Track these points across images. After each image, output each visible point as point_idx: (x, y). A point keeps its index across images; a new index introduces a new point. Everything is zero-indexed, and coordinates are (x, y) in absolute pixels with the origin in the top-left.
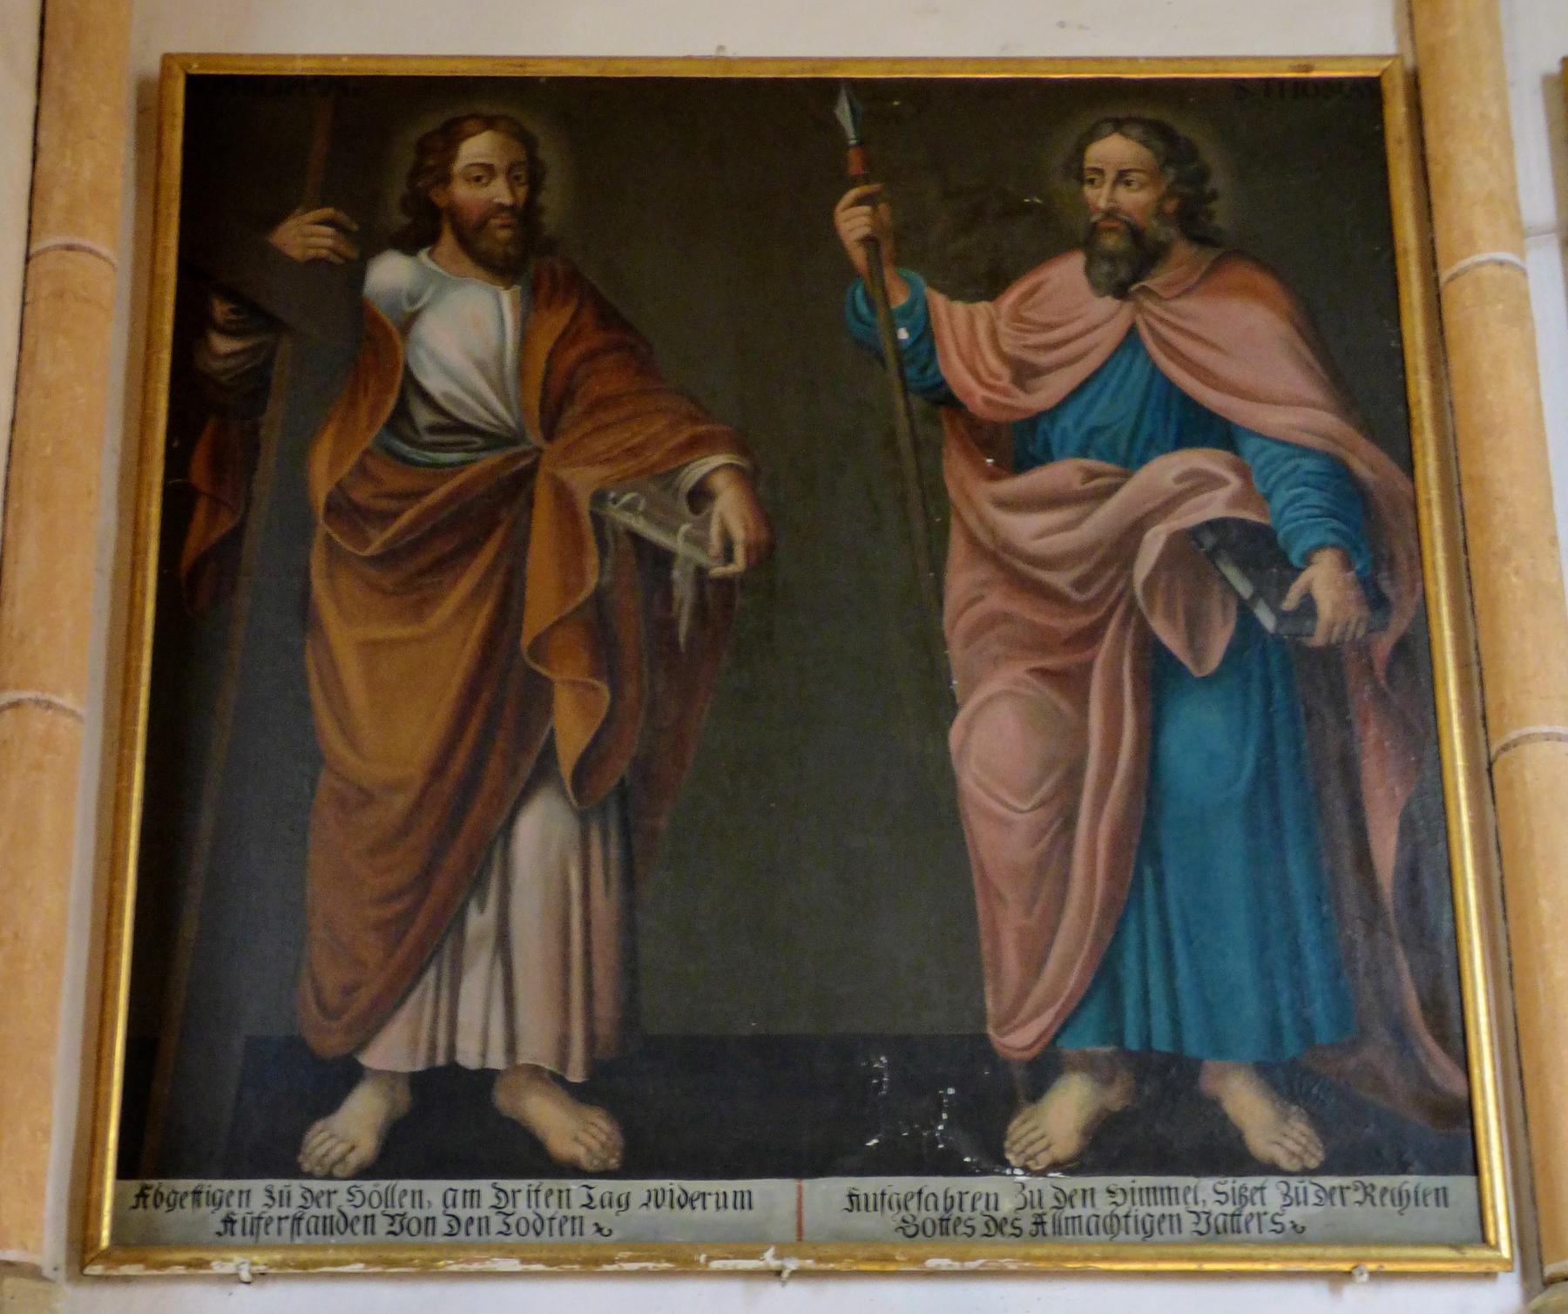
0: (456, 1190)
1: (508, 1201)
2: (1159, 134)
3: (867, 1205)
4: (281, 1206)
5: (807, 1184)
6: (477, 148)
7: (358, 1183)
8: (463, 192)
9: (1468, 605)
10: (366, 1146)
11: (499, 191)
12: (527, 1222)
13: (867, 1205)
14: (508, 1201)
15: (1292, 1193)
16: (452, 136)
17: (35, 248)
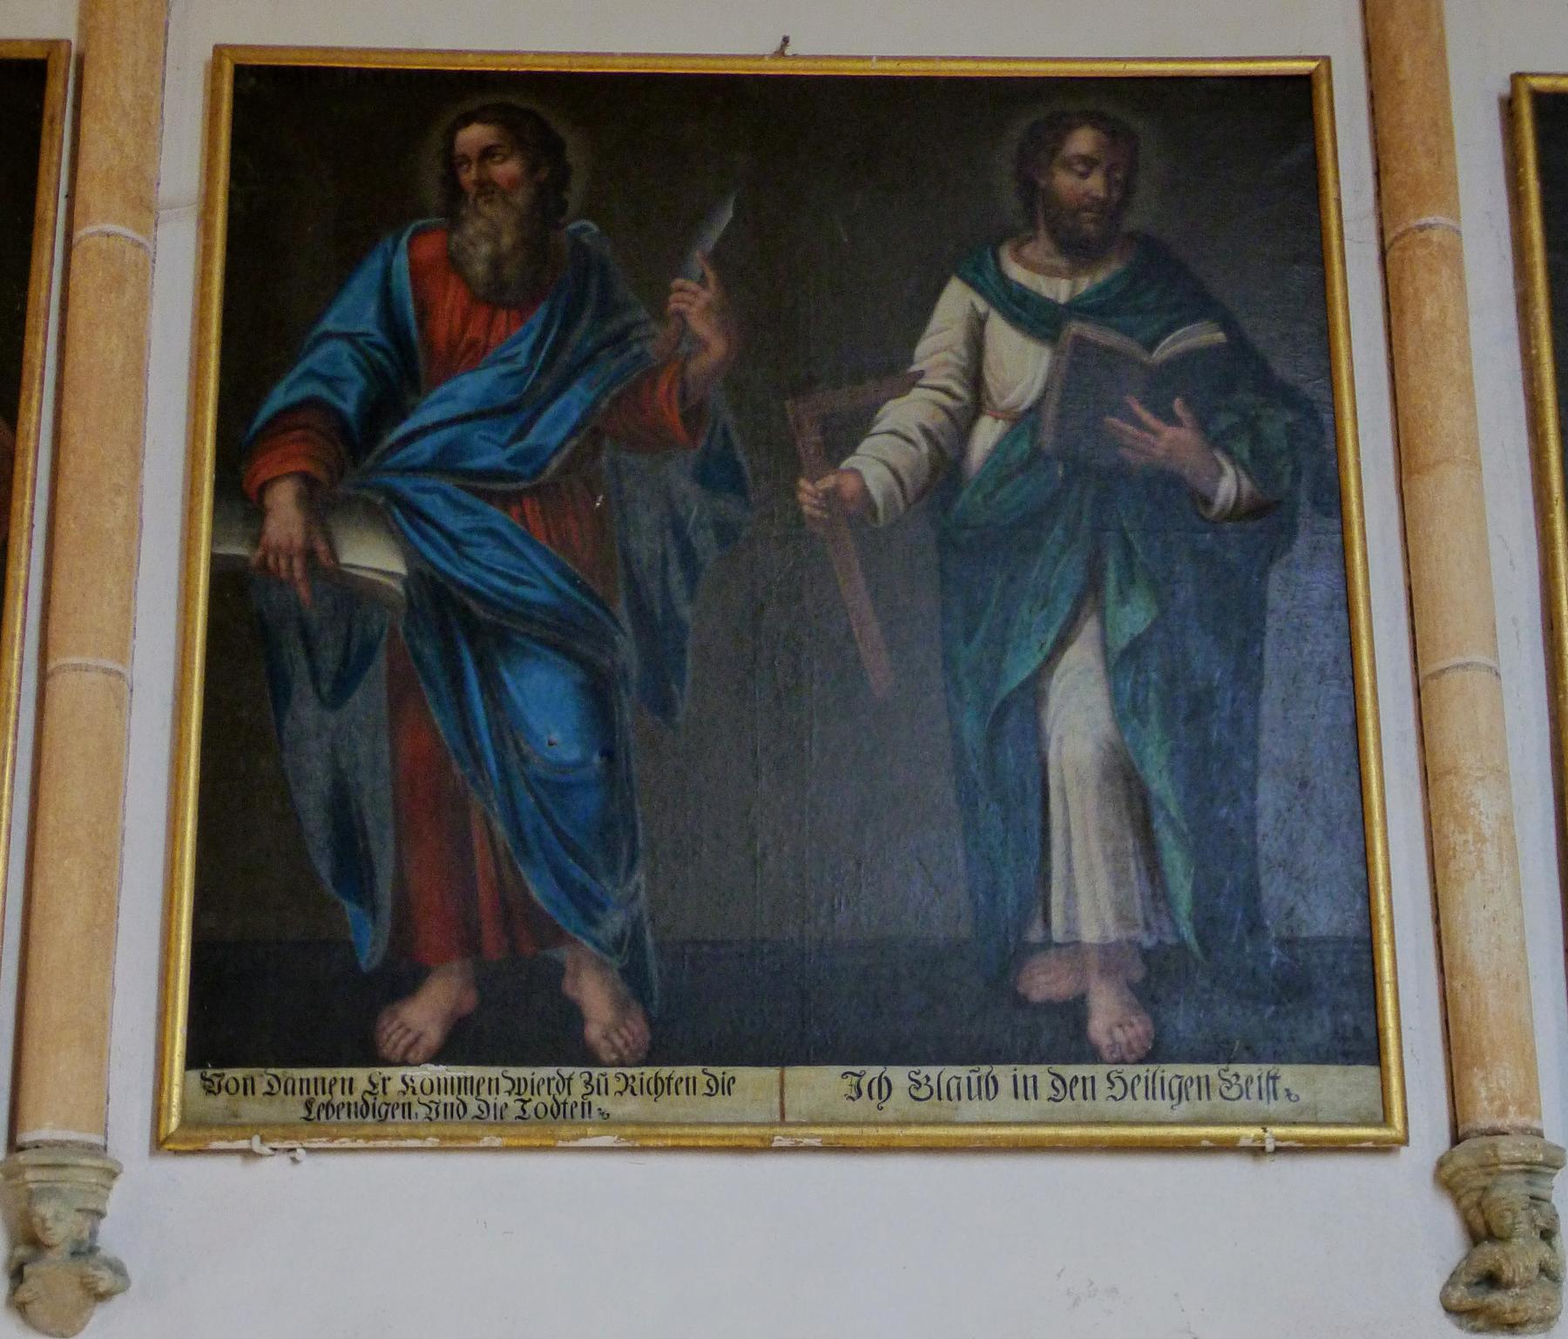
0: (960, 1078)
1: (1066, 1092)
2: (1114, 132)
3: (316, 1082)
4: (472, 1078)
5: (796, 1074)
6: (1083, 141)
7: (1119, 1067)
8: (1065, 182)
9: (22, 587)
10: (433, 1035)
11: (1095, 184)
12: (227, 1090)
13: (316, 1082)
14: (1066, 1092)
15: (594, 1082)
16: (1061, 127)
17: (1389, 237)
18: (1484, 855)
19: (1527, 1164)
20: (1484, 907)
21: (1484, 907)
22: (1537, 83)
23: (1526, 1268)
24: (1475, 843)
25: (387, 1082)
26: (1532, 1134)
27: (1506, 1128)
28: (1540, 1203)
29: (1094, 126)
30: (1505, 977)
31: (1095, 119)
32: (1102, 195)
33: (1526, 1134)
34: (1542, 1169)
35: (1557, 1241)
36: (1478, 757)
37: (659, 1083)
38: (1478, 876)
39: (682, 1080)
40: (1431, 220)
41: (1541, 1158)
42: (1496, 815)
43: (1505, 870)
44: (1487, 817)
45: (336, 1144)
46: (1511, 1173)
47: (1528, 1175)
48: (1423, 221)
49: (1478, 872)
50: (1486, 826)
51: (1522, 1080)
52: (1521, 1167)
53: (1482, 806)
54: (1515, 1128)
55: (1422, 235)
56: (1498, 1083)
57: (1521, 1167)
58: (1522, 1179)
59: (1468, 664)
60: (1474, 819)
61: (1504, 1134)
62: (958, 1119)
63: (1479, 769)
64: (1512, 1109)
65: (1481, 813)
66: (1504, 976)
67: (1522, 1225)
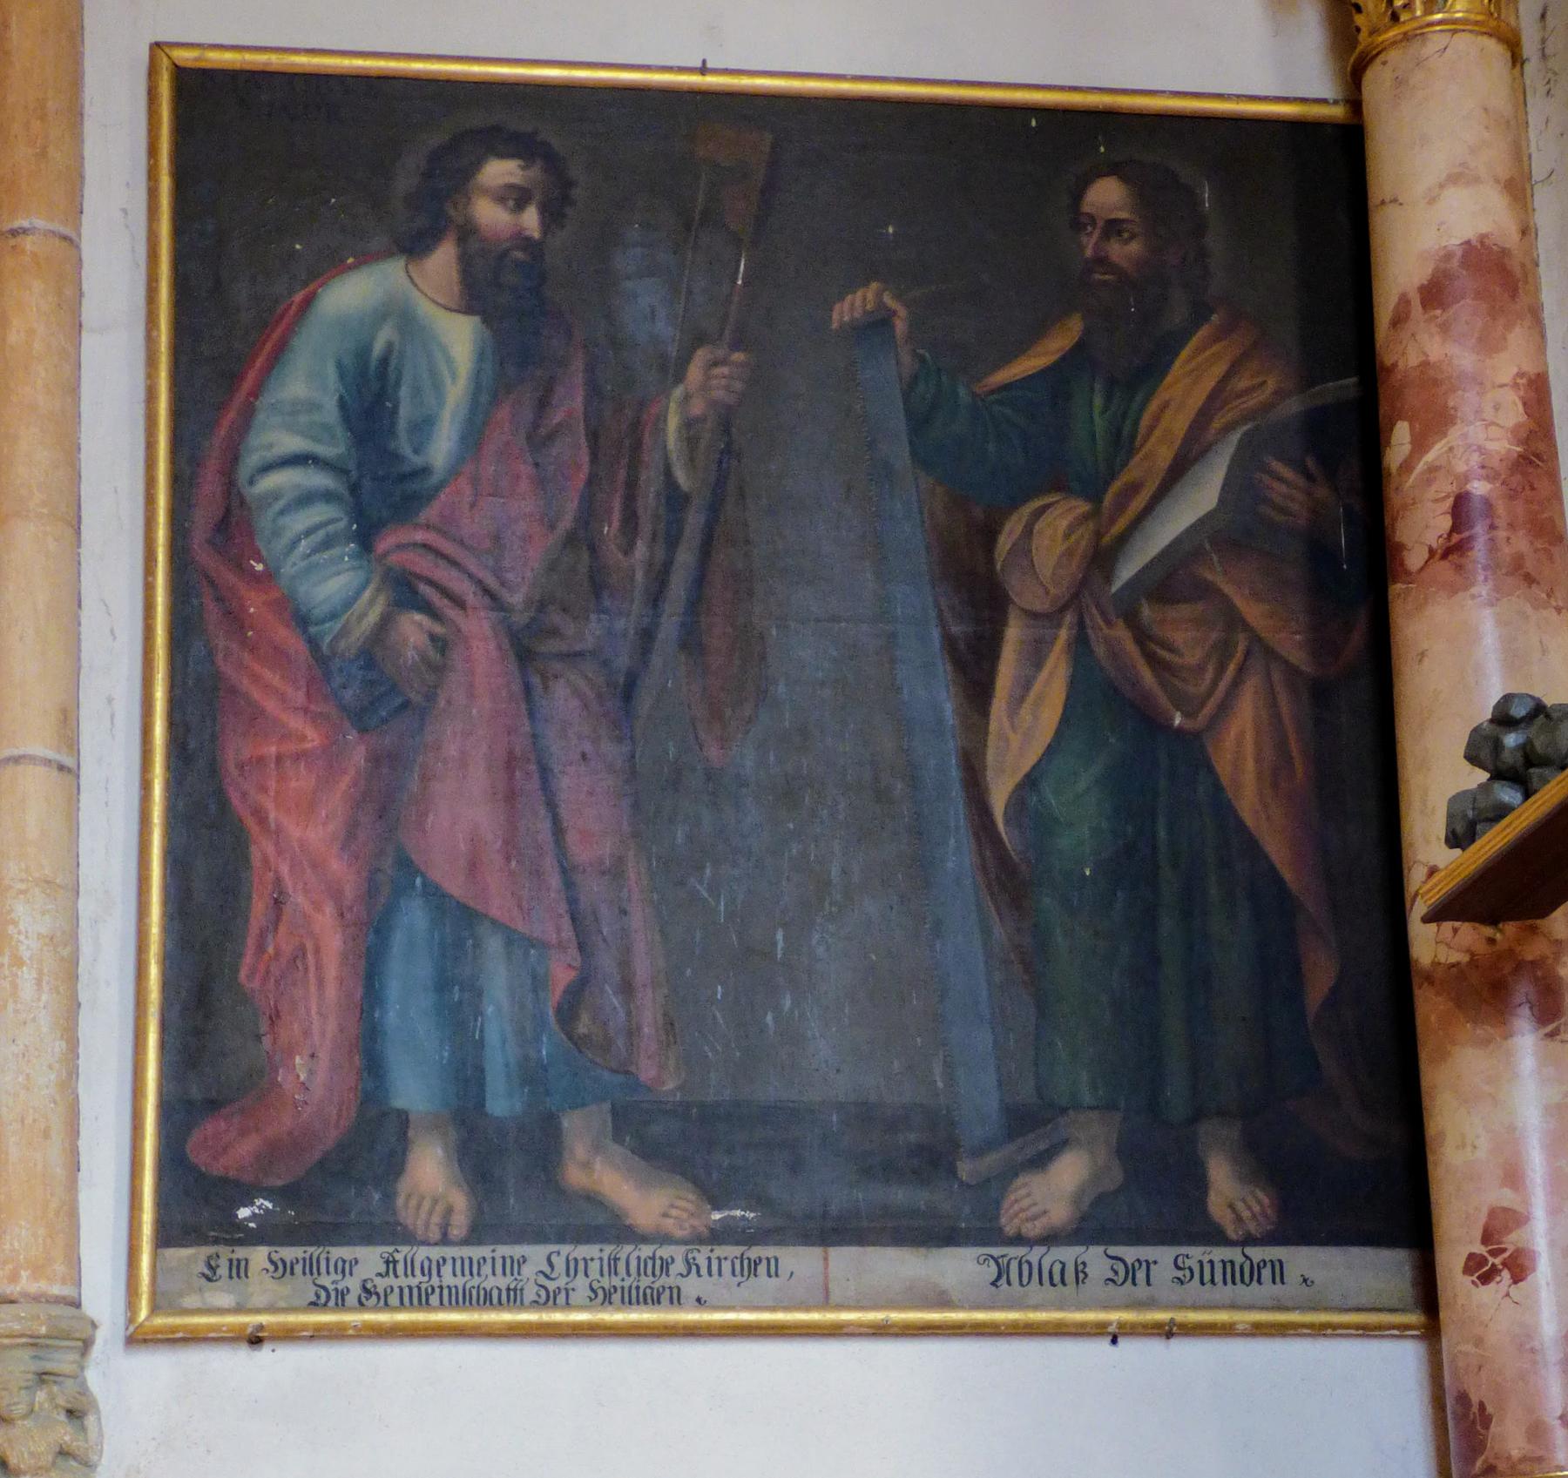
5: (837, 1254)
18: (19, 981)
19: (31, 1337)
20: (14, 1041)
21: (14, 1041)
22: (185, 57)
23: (32, 1454)
24: (10, 965)
25: (1152, 1266)
26: (47, 1301)
27: (15, 1296)
28: (60, 1379)
29: (1124, 179)
30: (31, 1122)
31: (523, 147)
32: (536, 235)
33: (40, 1302)
34: (49, 1342)
35: (90, 1420)
36: (23, 866)
37: (1025, 1267)
38: (11, 1007)
39: (760, 1260)
40: (25, 224)
41: (43, 1330)
42: (39, 934)
43: (44, 998)
44: (27, 937)
45: (1335, 1332)
46: (12, 1347)
47: (34, 1348)
48: (16, 224)
49: (11, 1000)
50: (25, 947)
51: (40, 1240)
52: (24, 1340)
53: (21, 923)
54: (26, 1295)
55: (12, 242)
56: (11, 1244)
57: (24, 1340)
58: (26, 1354)
59: (24, 757)
60: (12, 938)
61: (12, 1302)
62: (249, 1306)
63: (22, 881)
64: (24, 1274)
65: (19, 933)
66: (29, 1121)
67: (19, 1407)
